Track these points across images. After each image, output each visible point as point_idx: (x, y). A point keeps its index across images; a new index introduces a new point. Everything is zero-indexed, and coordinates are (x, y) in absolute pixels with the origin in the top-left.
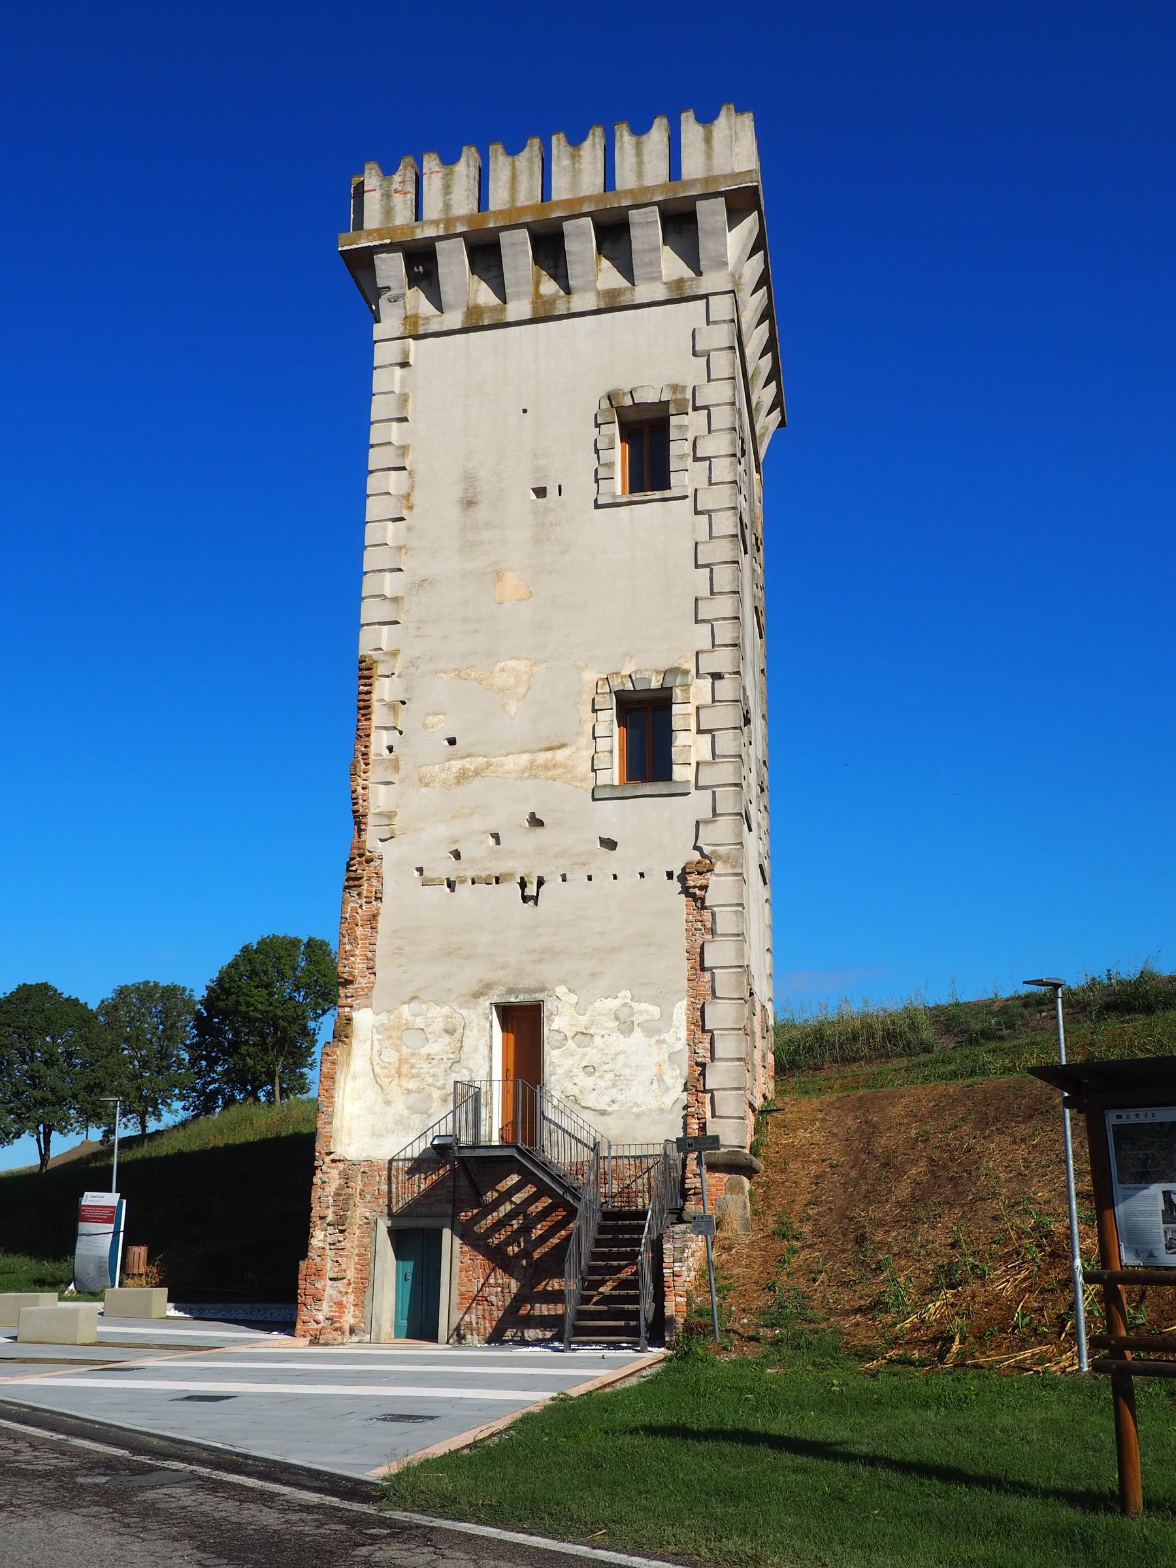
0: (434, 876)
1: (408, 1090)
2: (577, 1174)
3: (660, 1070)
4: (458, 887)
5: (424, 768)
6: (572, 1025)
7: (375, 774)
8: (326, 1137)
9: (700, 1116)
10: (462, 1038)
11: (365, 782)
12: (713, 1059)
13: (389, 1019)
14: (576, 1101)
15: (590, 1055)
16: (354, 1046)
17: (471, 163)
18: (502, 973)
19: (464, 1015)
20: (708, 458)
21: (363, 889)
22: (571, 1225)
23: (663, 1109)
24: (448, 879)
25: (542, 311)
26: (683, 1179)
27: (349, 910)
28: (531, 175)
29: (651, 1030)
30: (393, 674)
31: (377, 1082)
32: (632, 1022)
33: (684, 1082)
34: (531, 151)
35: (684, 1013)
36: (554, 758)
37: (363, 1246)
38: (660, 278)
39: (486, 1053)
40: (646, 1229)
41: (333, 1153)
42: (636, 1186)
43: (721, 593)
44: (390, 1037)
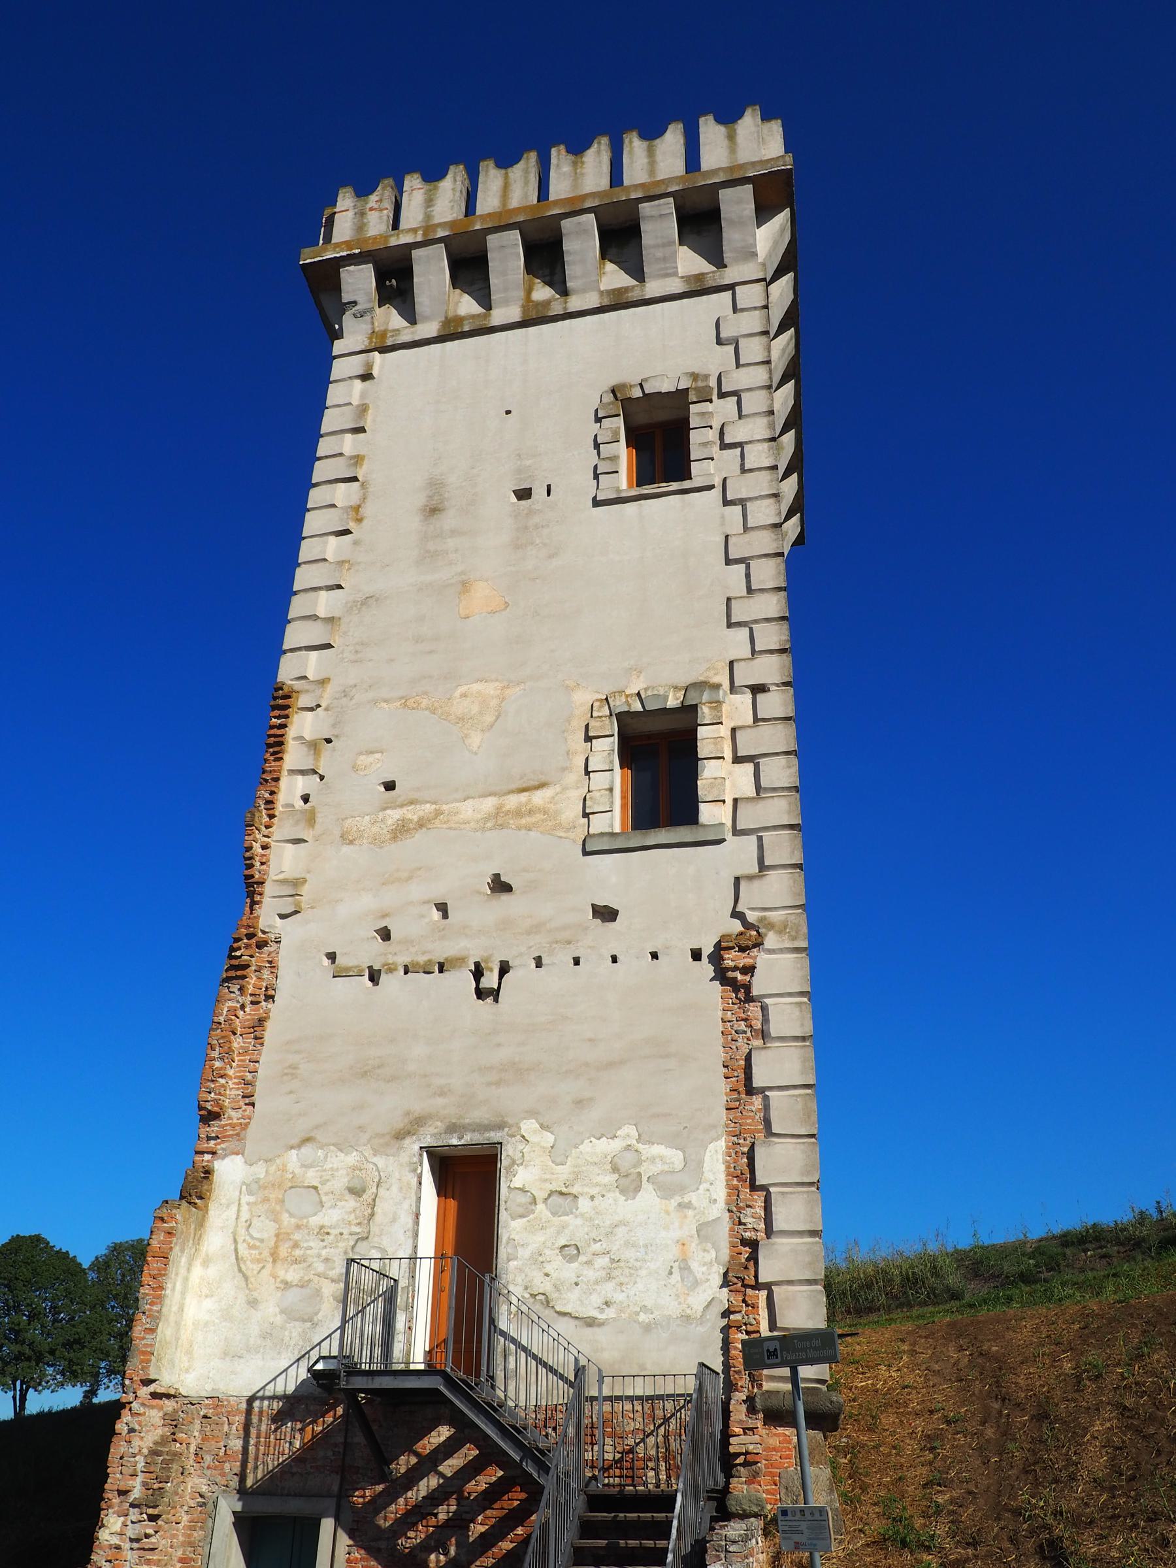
0: (351, 964)
1: (286, 1283)
2: (545, 1427)
3: (684, 1253)
4: (384, 978)
5: (349, 821)
6: (545, 1181)
7: (282, 829)
8: (144, 1353)
9: (750, 1328)
10: (374, 1200)
11: (266, 839)
12: (769, 1232)
13: (267, 1171)
14: (547, 1303)
15: (571, 1228)
16: (211, 1212)
17: (458, 178)
18: (440, 1101)
19: (380, 1166)
20: (740, 445)
21: (248, 983)
22: (533, 1517)
23: (688, 1317)
24: (370, 968)
25: (534, 312)
26: (726, 1435)
27: (225, 1013)
28: (526, 183)
29: (667, 1187)
30: (319, 706)
31: (240, 1270)
32: (640, 1174)
33: (722, 1271)
34: (527, 163)
35: (721, 1161)
36: (529, 801)
37: (190, 1544)
38: (675, 274)
39: (410, 1225)
40: (674, 1531)
41: (154, 1381)
42: (646, 1449)
43: (762, 590)
44: (266, 1200)
